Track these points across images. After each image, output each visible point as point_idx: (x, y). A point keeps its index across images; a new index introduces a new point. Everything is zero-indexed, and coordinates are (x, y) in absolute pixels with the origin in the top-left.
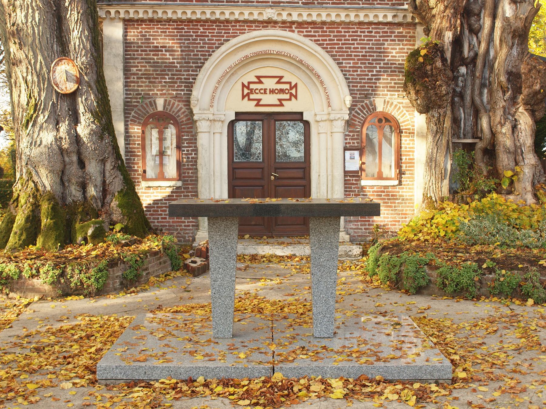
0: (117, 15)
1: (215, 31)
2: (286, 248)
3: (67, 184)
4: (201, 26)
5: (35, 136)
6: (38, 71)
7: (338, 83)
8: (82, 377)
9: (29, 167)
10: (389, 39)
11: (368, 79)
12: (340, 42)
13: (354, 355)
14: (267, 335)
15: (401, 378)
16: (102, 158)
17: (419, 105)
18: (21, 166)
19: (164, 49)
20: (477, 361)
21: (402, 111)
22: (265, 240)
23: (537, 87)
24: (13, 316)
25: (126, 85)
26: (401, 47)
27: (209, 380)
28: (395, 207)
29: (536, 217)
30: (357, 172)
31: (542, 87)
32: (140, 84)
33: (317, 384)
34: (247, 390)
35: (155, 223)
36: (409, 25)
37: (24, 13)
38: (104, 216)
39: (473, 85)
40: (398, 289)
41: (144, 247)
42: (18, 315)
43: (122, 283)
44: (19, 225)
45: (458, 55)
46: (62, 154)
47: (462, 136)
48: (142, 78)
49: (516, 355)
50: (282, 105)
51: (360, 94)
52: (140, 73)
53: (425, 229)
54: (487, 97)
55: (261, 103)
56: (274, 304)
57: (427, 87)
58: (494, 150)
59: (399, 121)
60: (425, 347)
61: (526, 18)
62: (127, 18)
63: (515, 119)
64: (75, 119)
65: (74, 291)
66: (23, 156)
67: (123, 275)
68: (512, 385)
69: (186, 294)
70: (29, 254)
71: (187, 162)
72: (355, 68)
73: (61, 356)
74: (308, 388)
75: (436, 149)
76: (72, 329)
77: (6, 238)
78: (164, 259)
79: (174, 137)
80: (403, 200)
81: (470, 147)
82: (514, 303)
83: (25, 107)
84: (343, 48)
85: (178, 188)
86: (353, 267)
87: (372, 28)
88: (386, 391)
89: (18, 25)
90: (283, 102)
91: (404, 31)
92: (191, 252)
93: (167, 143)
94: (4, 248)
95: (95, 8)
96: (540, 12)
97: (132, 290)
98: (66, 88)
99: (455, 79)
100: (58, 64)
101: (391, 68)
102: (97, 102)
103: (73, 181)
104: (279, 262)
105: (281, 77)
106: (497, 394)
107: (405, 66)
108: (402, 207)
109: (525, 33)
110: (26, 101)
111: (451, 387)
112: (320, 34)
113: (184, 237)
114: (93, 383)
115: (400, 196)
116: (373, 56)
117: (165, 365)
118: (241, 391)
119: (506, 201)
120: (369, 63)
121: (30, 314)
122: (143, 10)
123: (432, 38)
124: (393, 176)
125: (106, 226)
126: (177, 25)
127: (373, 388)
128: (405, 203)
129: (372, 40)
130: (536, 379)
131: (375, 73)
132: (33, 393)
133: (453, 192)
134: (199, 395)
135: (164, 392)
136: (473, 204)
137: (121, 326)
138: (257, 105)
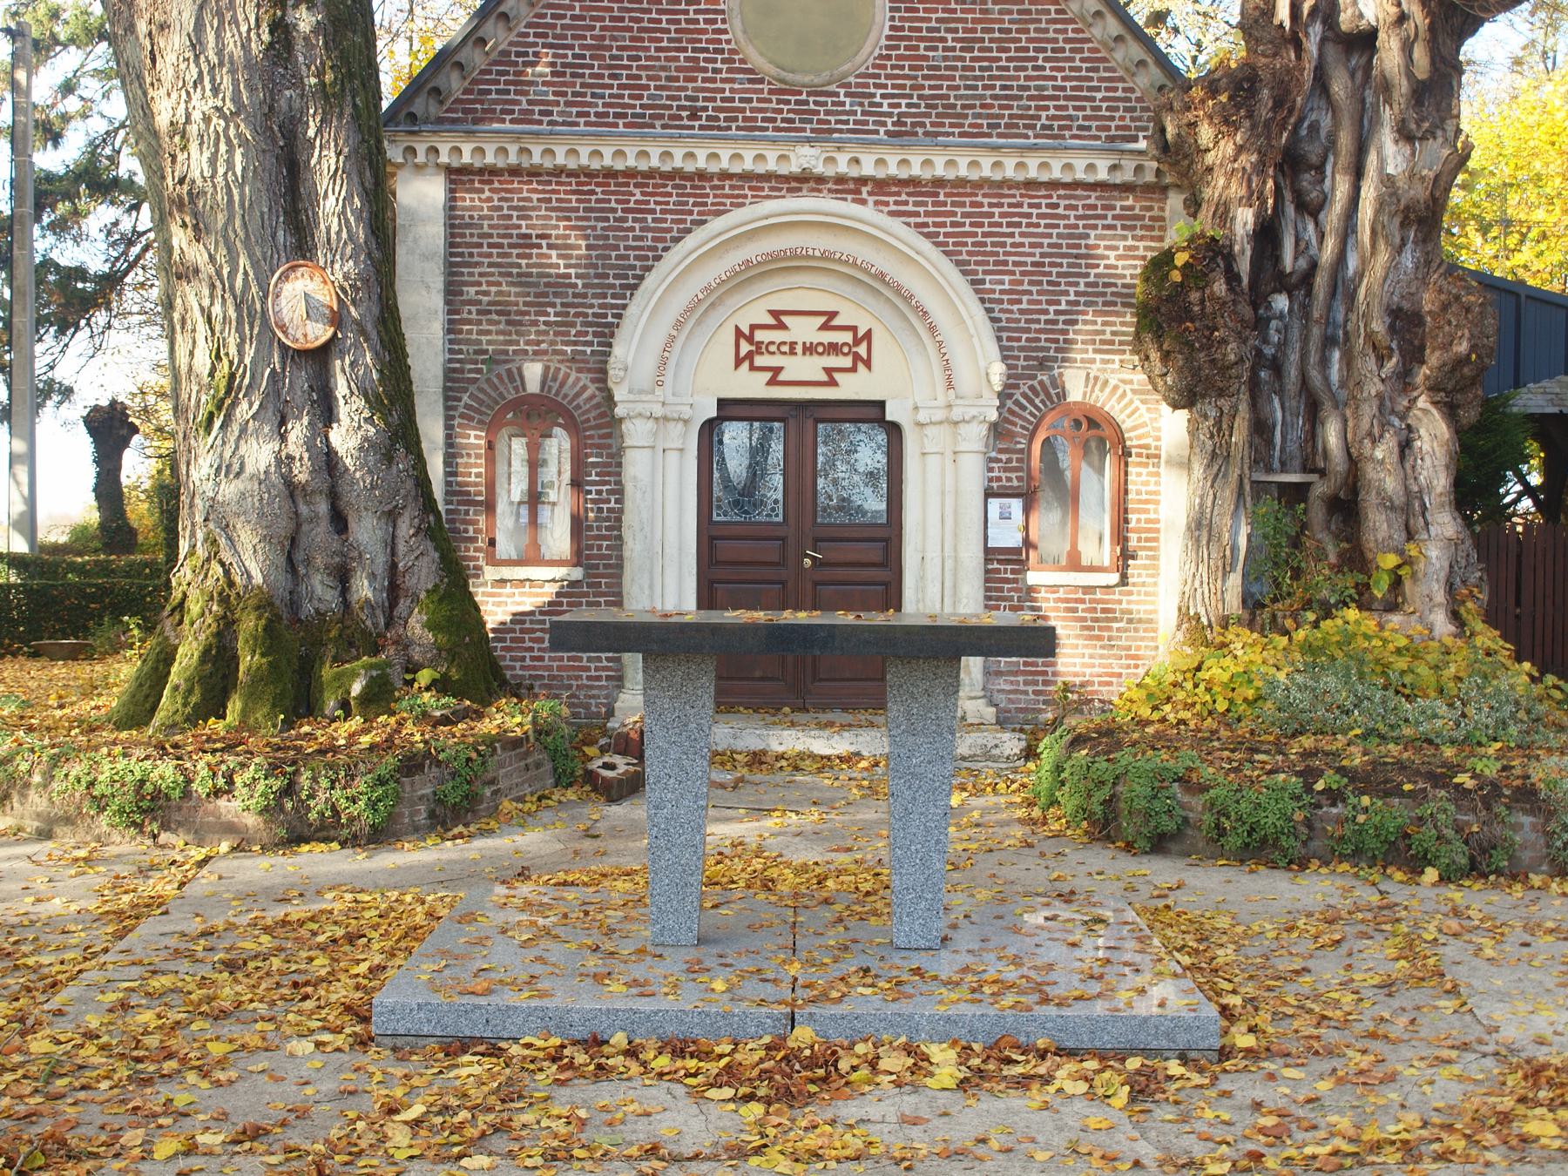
0: (432, 157)
1: (672, 200)
2: (836, 737)
3: (302, 570)
4: (636, 186)
5: (227, 454)
6: (238, 292)
7: (972, 331)
8: (338, 1030)
9: (211, 525)
10: (1100, 222)
11: (1047, 322)
12: (979, 230)
13: (987, 990)
14: (780, 941)
15: (1098, 1044)
16: (390, 507)
17: (1170, 389)
18: (193, 525)
19: (544, 243)
20: (1285, 1009)
21: (1131, 402)
22: (786, 715)
23: (1462, 347)
24: (168, 887)
25: (451, 328)
26: (1130, 242)
27: (638, 1041)
28: (1110, 638)
29: (1453, 669)
30: (1017, 551)
31: (1473, 348)
32: (485, 327)
33: (895, 1054)
34: (728, 1066)
35: (515, 670)
36: (1148, 189)
37: (207, 154)
38: (392, 650)
39: (1305, 340)
40: (1109, 839)
41: (487, 727)
42: (182, 885)
43: (432, 815)
44: (185, 669)
45: (1268, 265)
46: (292, 495)
47: (1276, 465)
48: (489, 312)
49: (1381, 998)
50: (832, 383)
51: (1026, 358)
52: (486, 299)
53: (1181, 695)
54: (1340, 370)
55: (781, 377)
56: (803, 869)
57: (1190, 345)
58: (1356, 502)
59: (1124, 427)
60: (1160, 973)
61: (1437, 178)
62: (455, 164)
63: (1409, 427)
64: (326, 413)
65: (318, 830)
66: (197, 501)
67: (435, 793)
68: (1363, 1065)
69: (587, 844)
70: (209, 740)
71: (597, 519)
72: (1015, 294)
73: (286, 981)
74: (873, 1064)
75: (1211, 497)
76: (312, 919)
77: (151, 699)
78: (537, 756)
79: (567, 456)
80: (1130, 621)
81: (1298, 493)
82: (1390, 877)
83: (206, 380)
84: (985, 244)
85: (573, 584)
86: (1002, 786)
87: (1059, 197)
88: (1059, 1074)
89: (194, 182)
90: (837, 376)
91: (1138, 206)
92: (602, 742)
93: (549, 473)
94: (147, 724)
95: (379, 142)
96: (1471, 164)
97: (456, 831)
98: (305, 336)
99: (1260, 324)
100: (287, 278)
101: (1104, 294)
102: (380, 372)
103: (319, 561)
104: (820, 770)
105: (833, 315)
106: (1324, 1086)
107: (1138, 290)
108: (1127, 638)
109: (1434, 213)
110: (209, 366)
111: (1217, 1068)
112: (930, 208)
113: (587, 707)
114: (363, 1043)
115: (1123, 612)
116: (1061, 265)
117: (534, 1003)
118: (714, 1067)
119: (1381, 627)
120: (1049, 283)
121: (210, 883)
122: (495, 146)
123: (1205, 223)
124: (1107, 563)
125: (396, 675)
126: (578, 184)
127: (1029, 1067)
128: (1136, 630)
129: (1058, 226)
130: (1424, 1054)
131: (1063, 307)
132: (222, 1063)
133: (1252, 603)
134: (614, 1076)
135: (532, 1067)
136: (1300, 635)
137: (430, 914)
138: (773, 382)
